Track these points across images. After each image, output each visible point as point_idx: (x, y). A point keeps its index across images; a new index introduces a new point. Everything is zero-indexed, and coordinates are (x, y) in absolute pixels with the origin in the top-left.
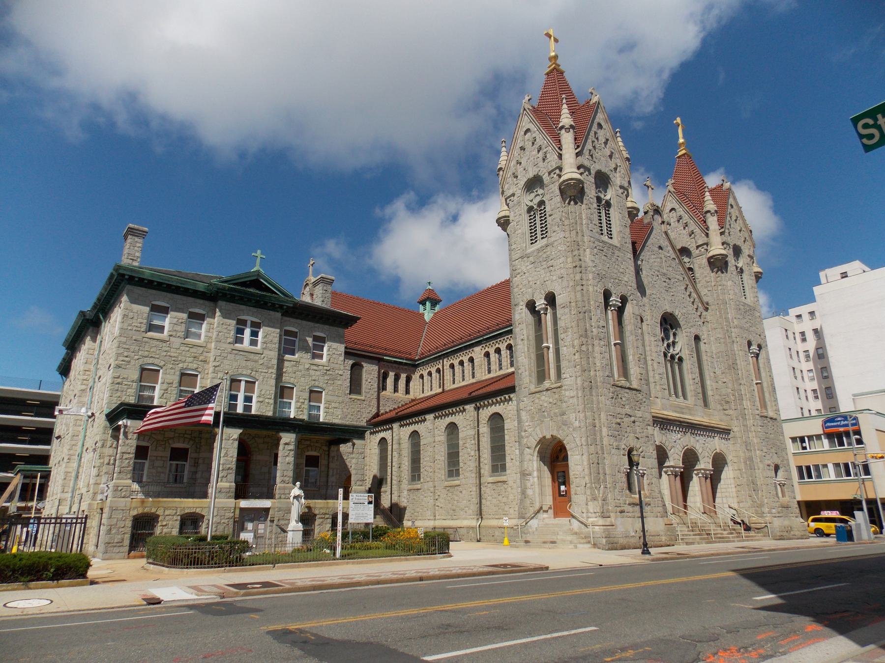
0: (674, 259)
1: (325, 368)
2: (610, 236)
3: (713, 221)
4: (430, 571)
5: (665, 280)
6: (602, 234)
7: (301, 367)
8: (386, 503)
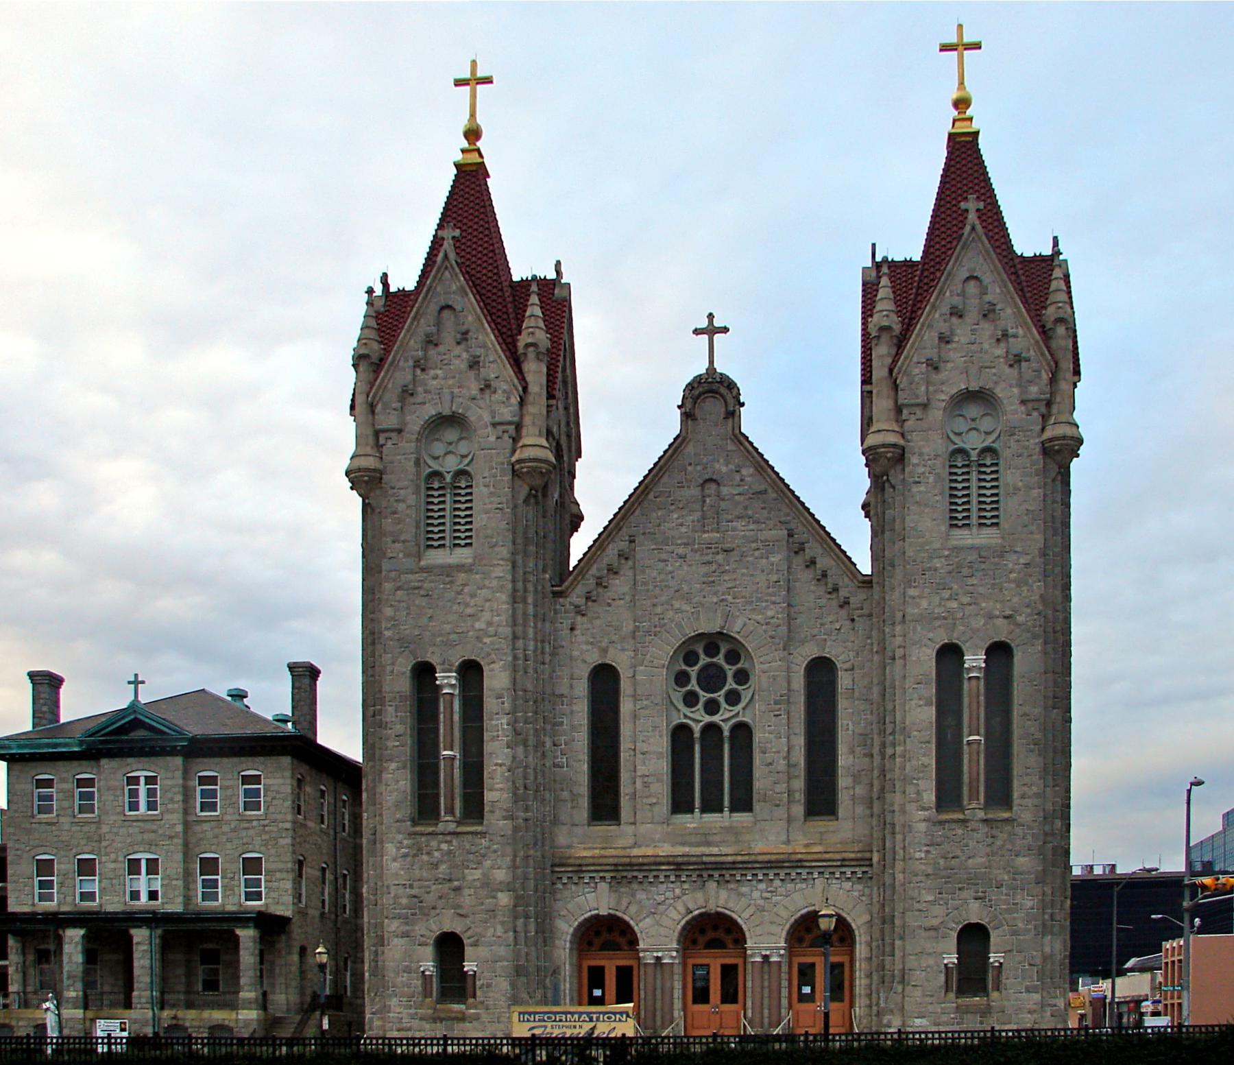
1: (262, 822)
7: (226, 828)
8: (918, 931)
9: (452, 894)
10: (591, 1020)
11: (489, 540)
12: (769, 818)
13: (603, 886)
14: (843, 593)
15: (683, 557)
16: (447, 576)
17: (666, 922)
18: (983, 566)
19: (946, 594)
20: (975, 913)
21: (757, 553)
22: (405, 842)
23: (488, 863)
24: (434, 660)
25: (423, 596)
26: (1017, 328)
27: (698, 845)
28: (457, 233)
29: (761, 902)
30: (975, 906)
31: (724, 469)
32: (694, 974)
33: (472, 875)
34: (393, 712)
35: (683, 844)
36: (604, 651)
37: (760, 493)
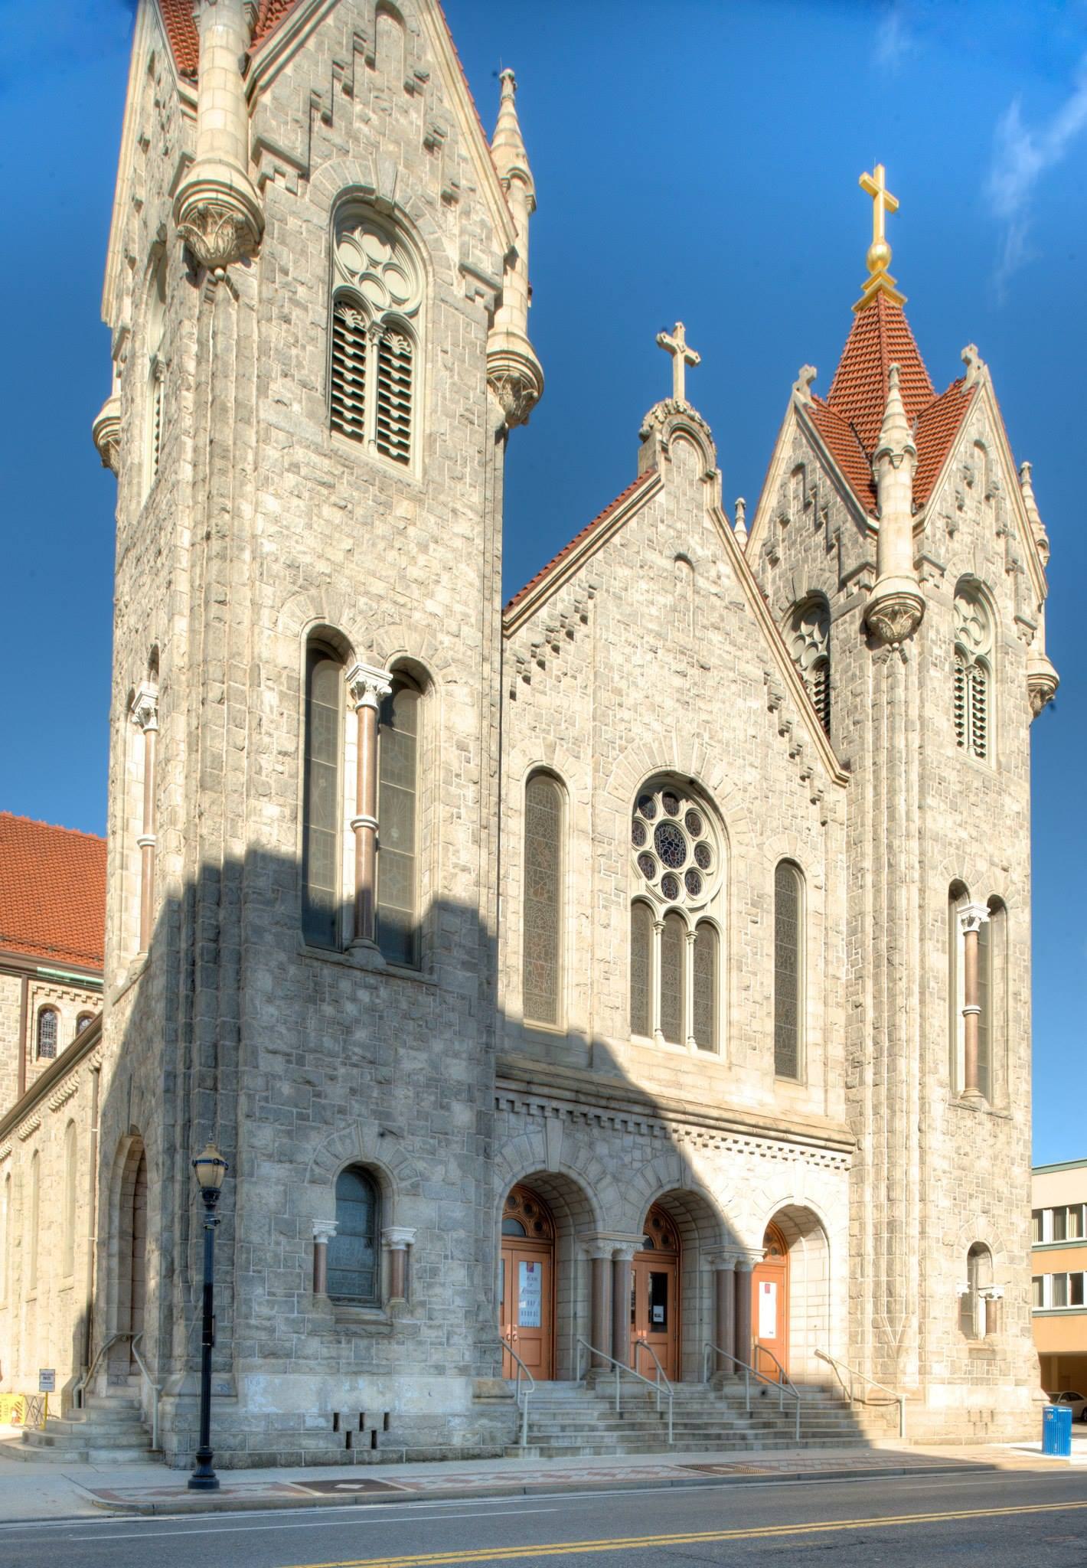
0: (740, 607)
2: (979, 750)
3: (897, 483)
4: (616, 1471)
5: (682, 667)
6: (960, 744)
13: (555, 1125)
17: (633, 1195)
24: (355, 634)
30: (982, 1221)
36: (551, 748)
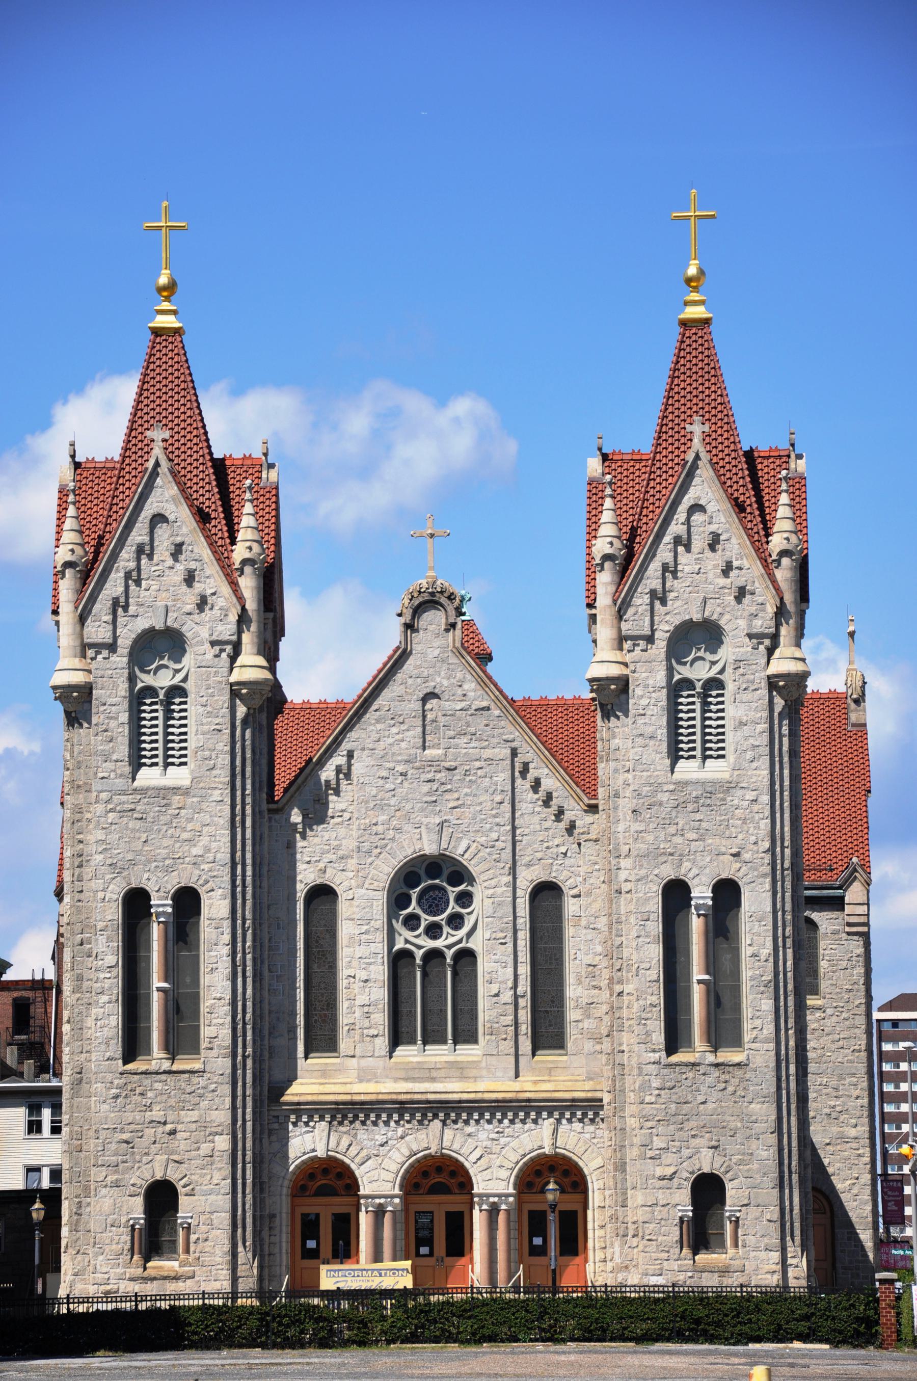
9: (167, 1138)
10: (381, 1276)
11: (207, 762)
12: (495, 1053)
14: (568, 816)
15: (403, 774)
16: (164, 798)
18: (708, 801)
19: (672, 829)
20: (707, 1163)
21: (480, 772)
22: (116, 1082)
23: (204, 1104)
25: (136, 819)
26: (742, 559)
27: (421, 1080)
28: (167, 434)
29: (489, 1143)
31: (445, 683)
32: (416, 1222)
33: (187, 1116)
34: (104, 941)
35: (406, 1079)
37: (483, 709)
